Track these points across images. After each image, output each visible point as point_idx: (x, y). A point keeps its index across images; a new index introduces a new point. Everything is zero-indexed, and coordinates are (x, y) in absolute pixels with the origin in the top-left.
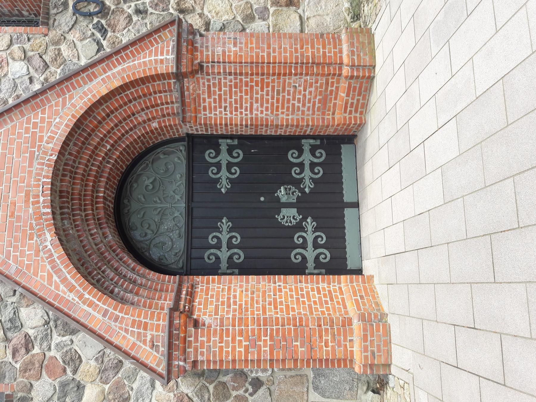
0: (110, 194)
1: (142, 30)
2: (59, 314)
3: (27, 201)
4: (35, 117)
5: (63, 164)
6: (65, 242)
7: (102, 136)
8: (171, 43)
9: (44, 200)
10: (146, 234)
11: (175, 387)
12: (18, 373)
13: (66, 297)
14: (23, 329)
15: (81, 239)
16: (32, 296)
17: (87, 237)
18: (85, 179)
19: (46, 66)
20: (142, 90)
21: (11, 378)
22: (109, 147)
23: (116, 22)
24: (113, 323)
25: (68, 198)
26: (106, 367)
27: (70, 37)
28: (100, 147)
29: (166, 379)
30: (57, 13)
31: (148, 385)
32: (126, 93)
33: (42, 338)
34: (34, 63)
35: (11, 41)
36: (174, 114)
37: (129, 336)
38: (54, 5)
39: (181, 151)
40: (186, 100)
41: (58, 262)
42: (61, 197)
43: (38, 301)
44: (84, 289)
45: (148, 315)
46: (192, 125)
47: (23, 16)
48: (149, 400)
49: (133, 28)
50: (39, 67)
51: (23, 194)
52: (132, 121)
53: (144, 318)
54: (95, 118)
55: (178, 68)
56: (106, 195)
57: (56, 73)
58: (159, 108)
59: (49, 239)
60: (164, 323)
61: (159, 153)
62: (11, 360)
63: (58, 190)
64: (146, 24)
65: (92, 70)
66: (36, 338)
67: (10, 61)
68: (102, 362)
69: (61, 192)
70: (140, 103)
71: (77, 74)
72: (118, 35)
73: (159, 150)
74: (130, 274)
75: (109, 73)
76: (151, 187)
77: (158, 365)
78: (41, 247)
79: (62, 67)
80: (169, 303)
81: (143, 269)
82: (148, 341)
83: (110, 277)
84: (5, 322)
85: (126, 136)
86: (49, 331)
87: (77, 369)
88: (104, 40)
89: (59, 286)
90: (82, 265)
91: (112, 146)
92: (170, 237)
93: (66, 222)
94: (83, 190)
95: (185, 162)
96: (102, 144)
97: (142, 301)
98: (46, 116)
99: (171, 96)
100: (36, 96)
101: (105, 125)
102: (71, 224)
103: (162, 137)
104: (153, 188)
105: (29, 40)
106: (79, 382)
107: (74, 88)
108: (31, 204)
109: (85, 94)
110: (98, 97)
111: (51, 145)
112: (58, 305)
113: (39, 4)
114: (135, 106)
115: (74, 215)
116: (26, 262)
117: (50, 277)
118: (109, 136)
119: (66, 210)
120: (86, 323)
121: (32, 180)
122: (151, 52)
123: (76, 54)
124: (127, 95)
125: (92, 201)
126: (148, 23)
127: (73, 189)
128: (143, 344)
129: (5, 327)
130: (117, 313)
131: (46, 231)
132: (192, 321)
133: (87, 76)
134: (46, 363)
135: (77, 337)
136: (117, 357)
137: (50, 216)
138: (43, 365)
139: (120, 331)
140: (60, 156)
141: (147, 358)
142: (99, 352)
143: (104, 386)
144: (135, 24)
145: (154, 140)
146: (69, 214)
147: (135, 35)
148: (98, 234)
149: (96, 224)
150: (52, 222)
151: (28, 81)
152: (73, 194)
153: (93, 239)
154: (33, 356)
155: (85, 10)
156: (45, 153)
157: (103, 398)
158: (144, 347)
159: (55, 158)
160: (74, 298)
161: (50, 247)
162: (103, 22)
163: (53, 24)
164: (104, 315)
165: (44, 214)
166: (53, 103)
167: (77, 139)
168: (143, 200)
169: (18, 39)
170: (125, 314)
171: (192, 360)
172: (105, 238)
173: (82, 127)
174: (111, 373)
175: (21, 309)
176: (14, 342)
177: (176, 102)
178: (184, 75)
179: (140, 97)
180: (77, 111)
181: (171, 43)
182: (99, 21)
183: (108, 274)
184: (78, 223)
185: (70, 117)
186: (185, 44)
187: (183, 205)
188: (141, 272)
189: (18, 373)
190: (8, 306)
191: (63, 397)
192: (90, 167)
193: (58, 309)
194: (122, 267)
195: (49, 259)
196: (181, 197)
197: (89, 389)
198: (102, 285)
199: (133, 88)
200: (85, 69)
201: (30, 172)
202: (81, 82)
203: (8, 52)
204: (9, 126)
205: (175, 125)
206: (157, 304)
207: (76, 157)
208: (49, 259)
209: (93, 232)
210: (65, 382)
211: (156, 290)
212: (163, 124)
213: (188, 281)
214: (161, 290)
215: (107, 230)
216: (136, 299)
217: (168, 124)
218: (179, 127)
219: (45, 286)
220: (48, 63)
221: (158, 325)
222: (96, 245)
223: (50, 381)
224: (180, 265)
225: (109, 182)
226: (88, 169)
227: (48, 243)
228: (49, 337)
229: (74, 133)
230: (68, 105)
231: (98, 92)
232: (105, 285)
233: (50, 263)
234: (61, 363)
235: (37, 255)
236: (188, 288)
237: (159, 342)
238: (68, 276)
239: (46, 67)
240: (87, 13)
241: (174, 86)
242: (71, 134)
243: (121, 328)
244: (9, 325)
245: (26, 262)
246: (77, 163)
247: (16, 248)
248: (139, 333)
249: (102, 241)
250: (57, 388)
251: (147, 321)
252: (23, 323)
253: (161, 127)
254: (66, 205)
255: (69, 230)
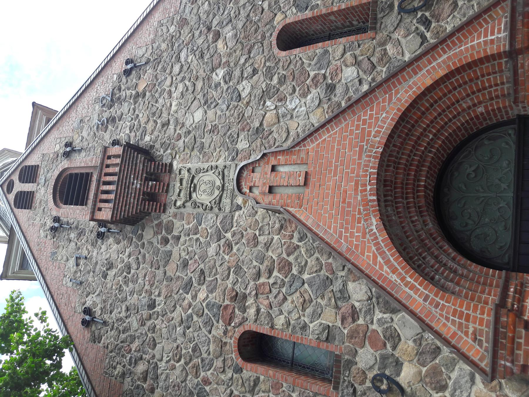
0: (431, 182)
1: (469, 13)
2: (382, 293)
3: (356, 190)
4: (366, 114)
5: (387, 155)
6: (388, 227)
7: (425, 126)
8: (504, 20)
9: (370, 189)
10: (467, 224)
11: (498, 387)
12: (346, 338)
13: (389, 277)
14: (350, 301)
15: (403, 225)
16: (359, 273)
17: (408, 224)
18: (407, 169)
19: (374, 67)
20: (469, 75)
21: (340, 341)
22: (431, 136)
23: (440, 12)
24: (434, 309)
25: (391, 187)
26: (424, 351)
27: (395, 36)
28: (422, 138)
29: (490, 376)
30: (384, 16)
31: (467, 378)
32: (451, 81)
33: (366, 311)
34: (363, 66)
35: (344, 50)
36: (503, 95)
37: (449, 324)
38: (380, 9)
39: (510, 135)
40: (520, 79)
41: (383, 245)
42: (385, 186)
43: (364, 278)
44: (407, 273)
45: (470, 307)
46: (526, 105)
47: (353, 25)
48: (467, 394)
49: (458, 13)
50: (368, 69)
51: (353, 184)
52: (456, 109)
53: (466, 309)
54: (419, 109)
55: (511, 45)
56: (427, 184)
57: (383, 72)
58: (486, 92)
59: (375, 223)
60: (488, 317)
61: (483, 139)
62: (340, 325)
63: (382, 179)
64: (473, 5)
65: (417, 64)
66: (360, 310)
67: (344, 67)
68: (420, 344)
69: (385, 181)
70: (465, 90)
71: (402, 69)
72: (442, 24)
73: (483, 136)
74: (450, 263)
75: (434, 64)
76: (473, 175)
77: (481, 360)
78: (368, 230)
79: (387, 66)
80: (493, 298)
81: (465, 259)
82: (470, 333)
83: (431, 264)
84: (336, 292)
85: (449, 124)
86: (372, 306)
87: (396, 346)
88: (428, 32)
89: (383, 266)
90: (404, 250)
91: (435, 135)
92: (494, 230)
93: (389, 209)
94: (406, 179)
95: (514, 147)
96: (424, 134)
97: (464, 292)
98: (374, 112)
99: (501, 77)
100: (366, 95)
101: (429, 115)
102: (394, 211)
103: (488, 121)
104: (476, 176)
105: (359, 46)
106: (398, 358)
107: (400, 83)
108: (359, 192)
109: (410, 87)
110: (423, 89)
111: (378, 139)
112: (382, 284)
113: (367, 11)
114: (459, 93)
115: (396, 203)
116: (355, 243)
117: (375, 258)
118: (431, 126)
119: (390, 198)
120: (407, 304)
121: (361, 170)
122: (486, 30)
123: (401, 51)
124: (452, 83)
125: (413, 189)
126: (475, 5)
127: (396, 178)
128: (465, 335)
129: (336, 297)
130: (437, 299)
131: (372, 216)
132: (523, 322)
133: (412, 70)
134: (368, 334)
135: (397, 316)
136: (434, 344)
137: (376, 203)
138: (367, 336)
139: (441, 318)
140: (386, 148)
141: (469, 350)
142: (418, 335)
143: (421, 368)
144: (461, 8)
145: (479, 125)
146: (392, 201)
147: (460, 20)
148: (419, 221)
149: (416, 212)
150: (377, 208)
151: (358, 83)
152: (396, 183)
153: (413, 225)
154: (358, 325)
155: (409, 7)
156: (372, 146)
157: (419, 379)
158: (465, 338)
159: (380, 150)
160: (397, 279)
161: (375, 230)
162: (427, 14)
163: (380, 27)
164: (425, 300)
165: (371, 201)
166: (381, 100)
167: (402, 131)
168: (464, 188)
169: (350, 48)
170: (446, 302)
171: (522, 363)
172: (426, 225)
173: (406, 119)
174: (428, 358)
175: (349, 282)
176: (343, 310)
177: (508, 82)
178: (520, 52)
179: (465, 83)
180: (402, 105)
181: (504, 20)
182: (423, 15)
183: (428, 261)
184: (400, 210)
185: (395, 111)
186: (521, 18)
187: (510, 194)
188: (462, 262)
189: (346, 338)
190: (339, 279)
191: (383, 368)
192: (412, 157)
193: (381, 287)
194: (442, 256)
195: (374, 242)
196: (507, 186)
197: (407, 367)
198: (423, 271)
199: (459, 75)
200: (410, 64)
201: (359, 164)
202: (407, 77)
203: (342, 60)
204: (343, 125)
205: (505, 107)
206: (480, 298)
207: (400, 148)
208: (374, 242)
209: (414, 219)
210: (385, 355)
211: (478, 282)
212: (490, 108)
213: (516, 278)
214: (485, 284)
215: (427, 218)
216: (457, 289)
217: (495, 107)
218: (509, 109)
219: (370, 265)
220: (375, 63)
221: (482, 319)
222: (417, 231)
223: (372, 351)
224: (506, 260)
225: (430, 172)
226: (410, 159)
227: (374, 227)
228: (372, 311)
229: (399, 126)
230: (394, 100)
231: (423, 84)
232: (426, 271)
233: (375, 245)
234: (382, 337)
235: (364, 237)
236: (516, 285)
237: (483, 337)
238: (392, 259)
239: (373, 68)
240: (412, 9)
241: (506, 65)
242: (396, 127)
243: (441, 315)
244: (339, 295)
245: (355, 243)
246: (400, 154)
247: (347, 229)
248: (460, 324)
249: (422, 229)
250: (378, 359)
251: (470, 312)
252: (350, 295)
253: (488, 112)
254: (390, 193)
255: (392, 216)
